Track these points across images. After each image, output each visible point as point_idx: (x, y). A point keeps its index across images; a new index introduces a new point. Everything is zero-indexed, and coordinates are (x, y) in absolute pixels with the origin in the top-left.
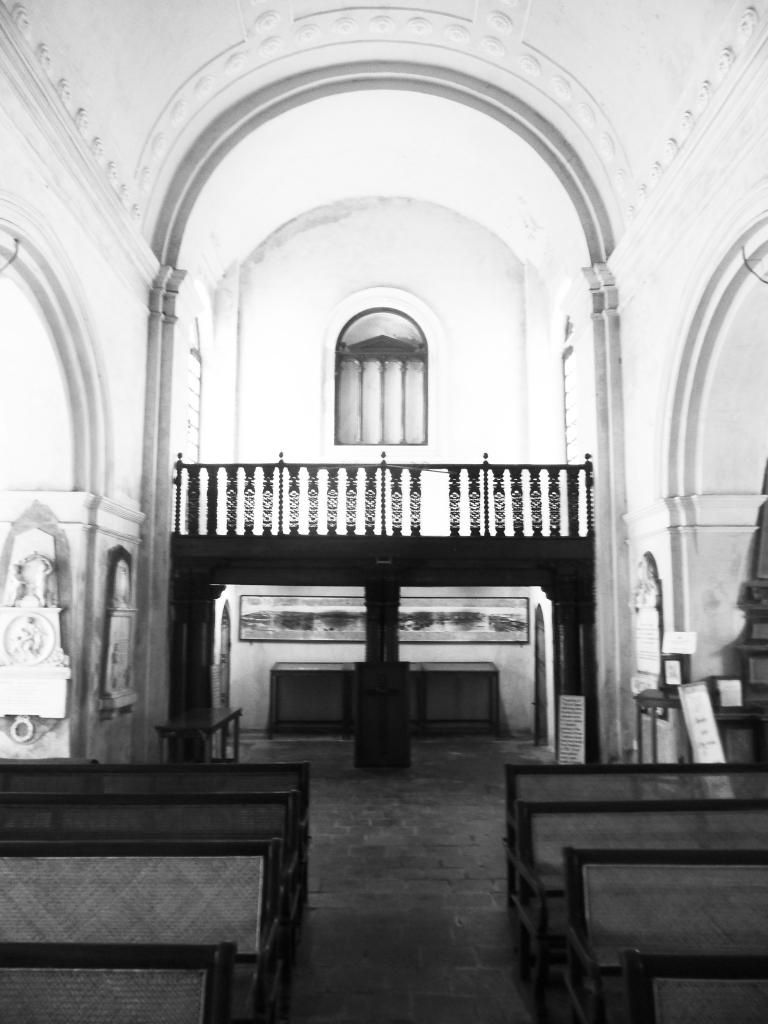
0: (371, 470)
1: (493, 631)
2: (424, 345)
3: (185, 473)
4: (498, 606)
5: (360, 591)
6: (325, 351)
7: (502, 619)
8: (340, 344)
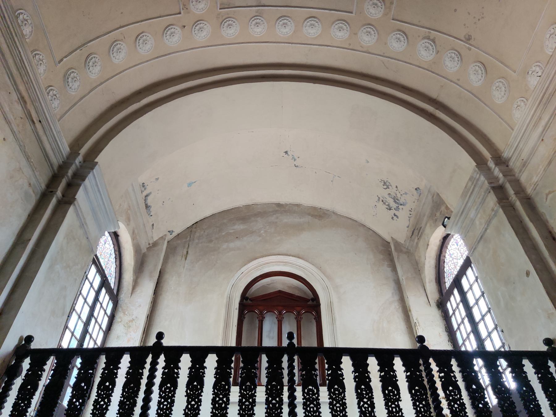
0: (275, 354)
2: (316, 298)
3: (26, 364)
6: (230, 299)
8: (244, 296)
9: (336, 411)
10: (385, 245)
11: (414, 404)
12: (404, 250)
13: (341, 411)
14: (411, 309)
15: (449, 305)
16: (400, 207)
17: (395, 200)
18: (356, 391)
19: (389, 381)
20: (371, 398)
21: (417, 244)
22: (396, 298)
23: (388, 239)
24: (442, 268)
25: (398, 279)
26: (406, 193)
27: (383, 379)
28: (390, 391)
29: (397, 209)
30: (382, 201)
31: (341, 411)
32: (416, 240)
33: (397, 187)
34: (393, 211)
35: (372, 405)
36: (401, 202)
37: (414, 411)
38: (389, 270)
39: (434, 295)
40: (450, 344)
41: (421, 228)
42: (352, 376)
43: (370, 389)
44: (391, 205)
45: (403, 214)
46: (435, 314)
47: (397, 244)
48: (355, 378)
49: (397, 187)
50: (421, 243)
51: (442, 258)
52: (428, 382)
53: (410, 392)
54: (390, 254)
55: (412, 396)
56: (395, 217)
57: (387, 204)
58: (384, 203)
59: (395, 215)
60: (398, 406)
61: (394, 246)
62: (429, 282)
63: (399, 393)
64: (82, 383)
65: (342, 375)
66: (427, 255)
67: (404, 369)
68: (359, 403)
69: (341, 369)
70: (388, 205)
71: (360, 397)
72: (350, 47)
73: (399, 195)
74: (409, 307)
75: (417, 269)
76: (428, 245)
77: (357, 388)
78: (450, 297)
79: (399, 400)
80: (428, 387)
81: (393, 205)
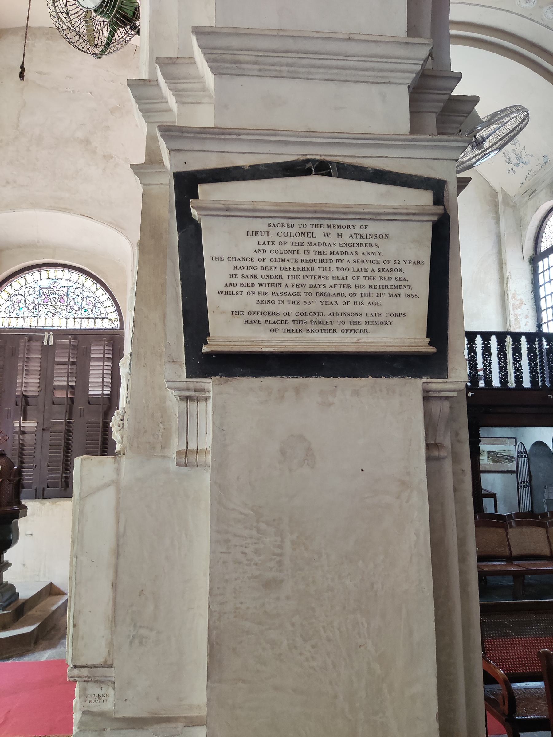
1: (491, 463)
4: (494, 444)
5: (90, 393)
7: (497, 454)
9: (486, 366)
10: (494, 194)
11: (529, 363)
12: (511, 204)
13: (489, 366)
14: (507, 263)
15: (540, 264)
16: (521, 164)
17: (518, 157)
18: (498, 356)
19: (517, 350)
20: (505, 360)
21: (527, 202)
22: (495, 251)
23: (497, 189)
24: (543, 228)
25: (500, 232)
26: (532, 156)
27: (513, 349)
28: (516, 356)
29: (517, 165)
30: (504, 153)
31: (489, 366)
32: (526, 199)
33: (524, 147)
34: (510, 166)
35: (506, 364)
36: (524, 161)
37: (528, 367)
38: (493, 222)
39: (528, 250)
40: (532, 293)
41: (536, 190)
42: (496, 347)
43: (505, 356)
44: (511, 160)
45: (522, 172)
46: (526, 267)
47: (506, 196)
48: (498, 348)
49: (524, 147)
50: (531, 203)
51: (546, 220)
52: (539, 351)
53: (528, 356)
54: (496, 205)
55: (529, 359)
56: (511, 171)
57: (508, 157)
58: (505, 156)
59: (512, 169)
60: (520, 364)
61: (503, 198)
62: (528, 240)
63: (521, 357)
64: (482, 389)
65: (490, 347)
66: (534, 216)
67: (526, 343)
68: (499, 362)
69: (490, 344)
70: (509, 159)
71: (500, 359)
72: (530, 17)
73: (523, 154)
74: (505, 260)
75: (520, 226)
76: (538, 209)
77: (499, 354)
78: (545, 258)
79: (521, 361)
80: (538, 353)
81: (514, 160)
